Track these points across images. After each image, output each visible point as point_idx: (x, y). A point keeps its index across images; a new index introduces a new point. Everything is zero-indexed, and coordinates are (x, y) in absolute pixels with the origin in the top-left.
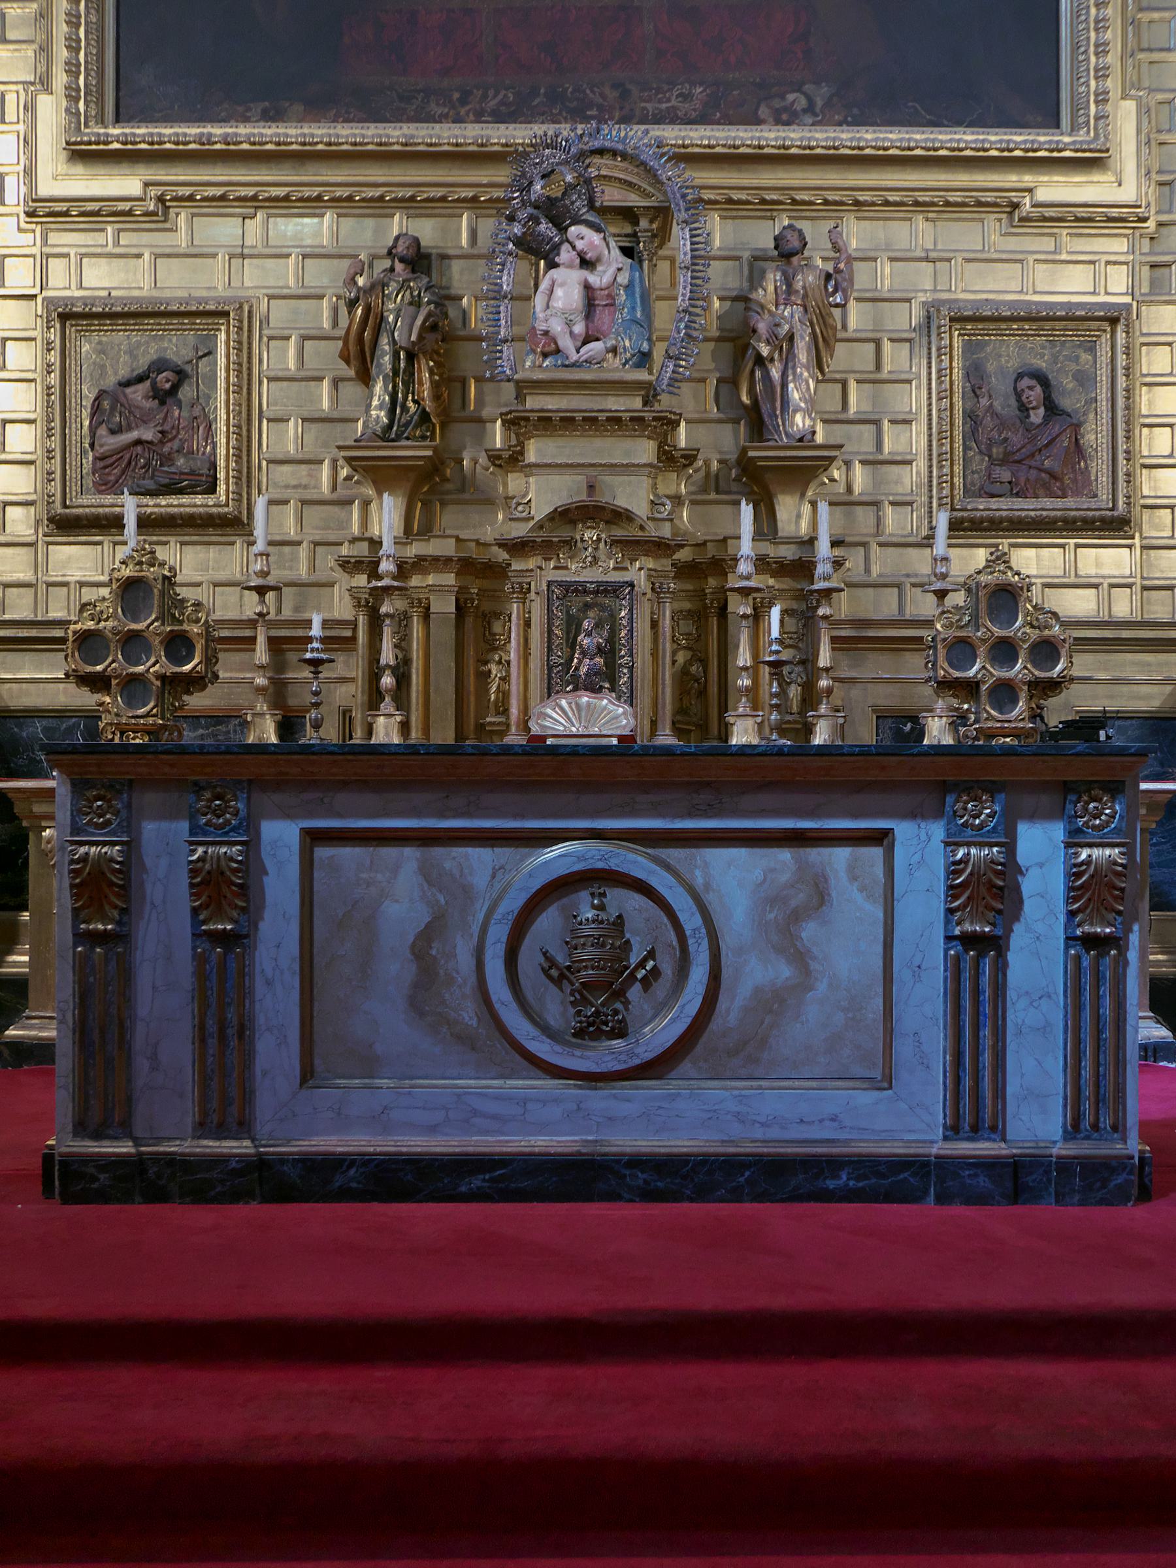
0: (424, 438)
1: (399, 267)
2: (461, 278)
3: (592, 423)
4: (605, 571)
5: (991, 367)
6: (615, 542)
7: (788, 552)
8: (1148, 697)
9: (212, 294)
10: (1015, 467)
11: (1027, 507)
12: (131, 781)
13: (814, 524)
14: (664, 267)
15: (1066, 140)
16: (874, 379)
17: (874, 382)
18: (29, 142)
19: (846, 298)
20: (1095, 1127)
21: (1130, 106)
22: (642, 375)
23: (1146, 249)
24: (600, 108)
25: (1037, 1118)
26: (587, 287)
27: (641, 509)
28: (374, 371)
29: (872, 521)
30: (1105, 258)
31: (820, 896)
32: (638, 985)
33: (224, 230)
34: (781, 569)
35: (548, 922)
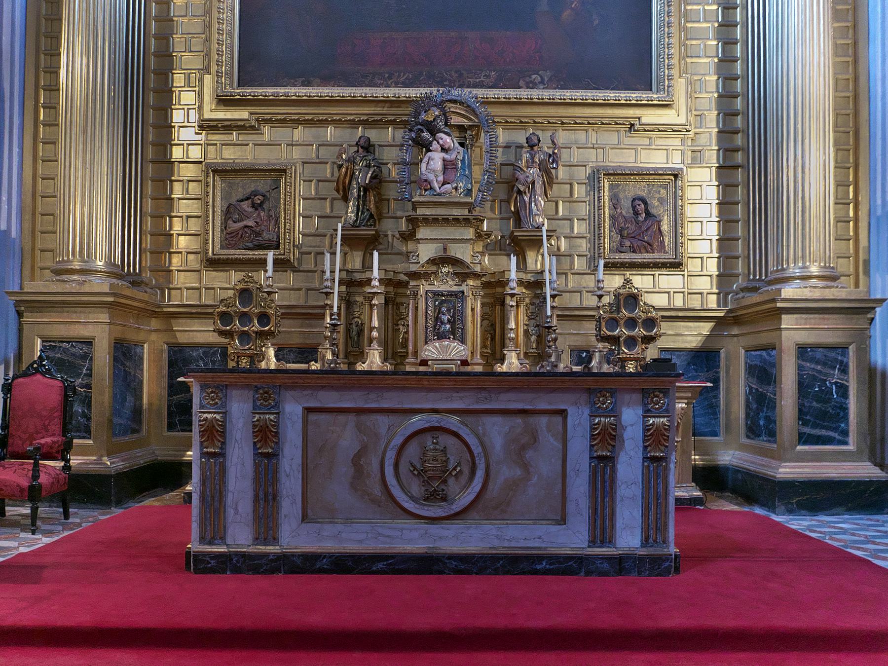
0: (371, 225)
1: (361, 150)
2: (390, 156)
3: (446, 221)
4: (450, 286)
5: (621, 196)
6: (456, 274)
7: (530, 277)
8: (691, 342)
9: (279, 162)
10: (632, 240)
11: (638, 258)
12: (227, 385)
13: (543, 264)
14: (478, 150)
15: (654, 97)
16: (570, 200)
17: (570, 202)
18: (200, 96)
19: (557, 165)
20: (655, 541)
21: (683, 81)
22: (469, 200)
23: (690, 144)
24: (450, 81)
25: (628, 539)
26: (444, 160)
27: (468, 259)
28: (349, 196)
29: (569, 263)
30: (672, 148)
31: (535, 439)
32: (453, 478)
33: (282, 134)
34: (529, 285)
35: (413, 450)
